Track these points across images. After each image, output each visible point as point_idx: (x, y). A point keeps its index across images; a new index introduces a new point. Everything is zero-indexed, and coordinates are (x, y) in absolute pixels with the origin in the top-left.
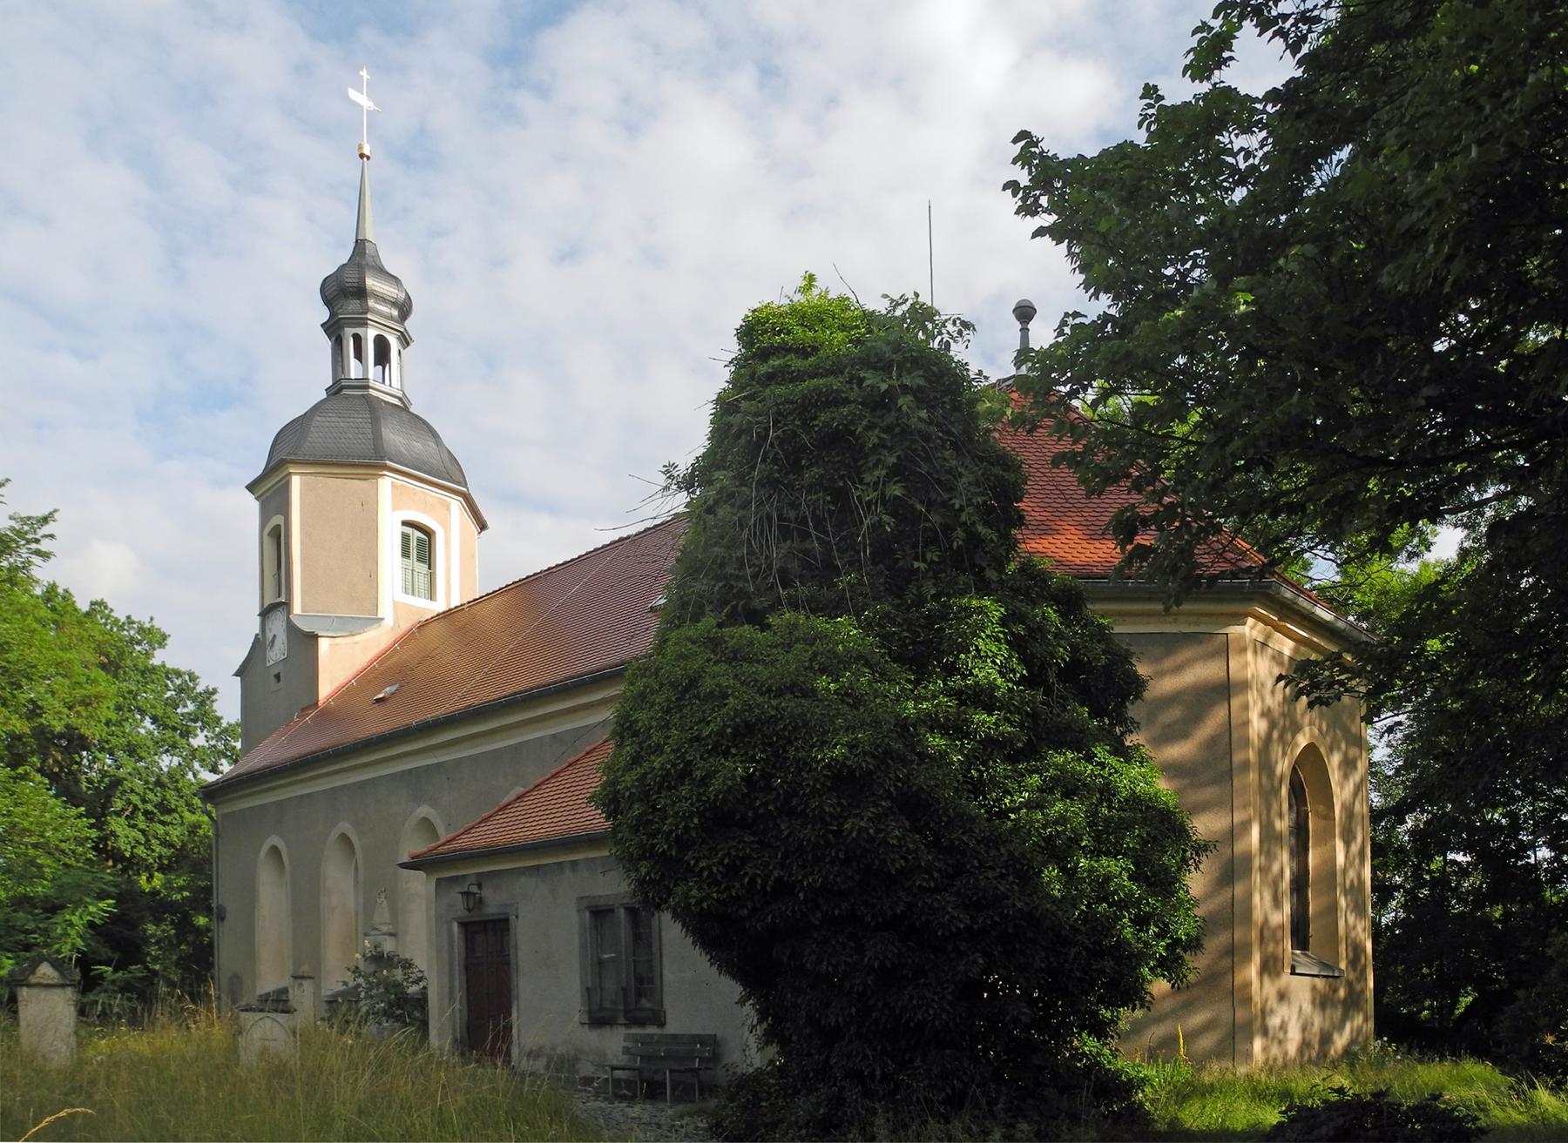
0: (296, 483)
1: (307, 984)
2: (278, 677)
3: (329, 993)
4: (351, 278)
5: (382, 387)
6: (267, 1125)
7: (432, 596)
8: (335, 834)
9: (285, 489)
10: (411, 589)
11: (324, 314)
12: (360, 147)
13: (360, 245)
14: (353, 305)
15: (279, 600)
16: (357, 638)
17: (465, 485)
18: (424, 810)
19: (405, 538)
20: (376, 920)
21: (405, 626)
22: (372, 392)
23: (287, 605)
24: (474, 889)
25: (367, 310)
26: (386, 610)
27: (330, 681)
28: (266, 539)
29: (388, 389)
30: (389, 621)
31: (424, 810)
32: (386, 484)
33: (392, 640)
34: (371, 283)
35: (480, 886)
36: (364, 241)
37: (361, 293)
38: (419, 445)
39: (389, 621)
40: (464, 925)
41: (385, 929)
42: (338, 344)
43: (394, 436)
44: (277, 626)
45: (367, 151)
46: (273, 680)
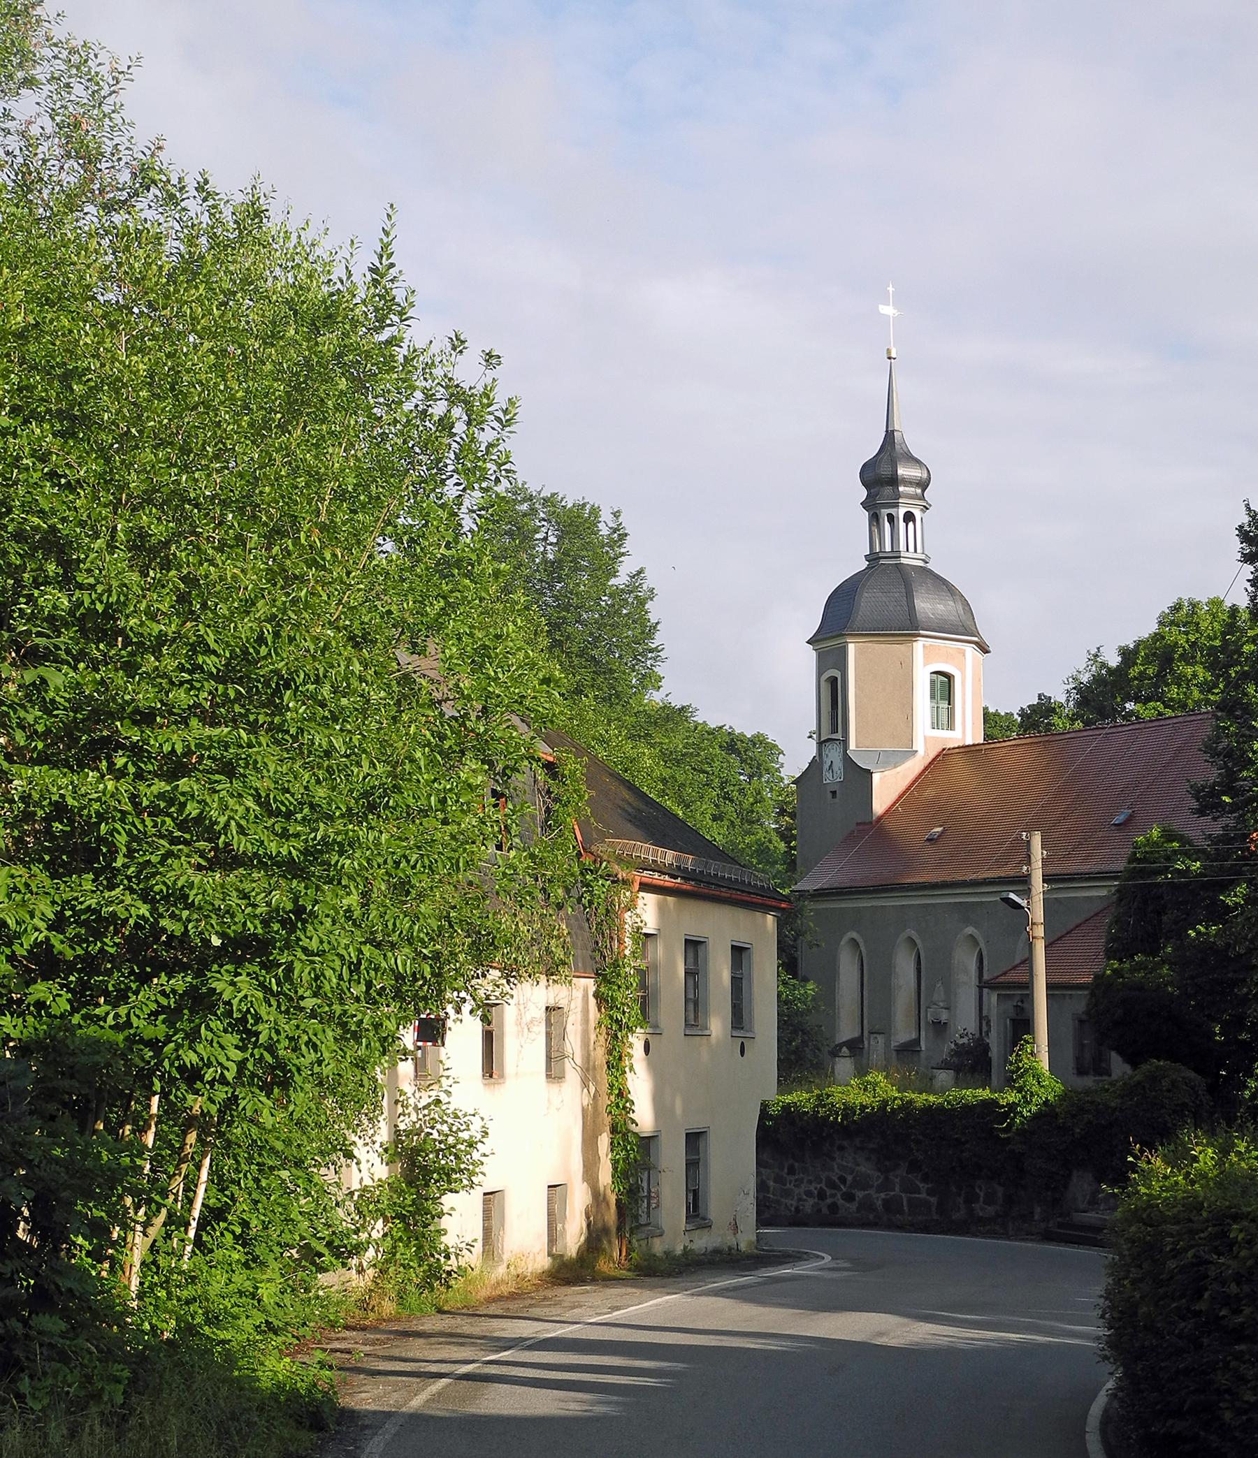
0: (851, 648)
1: (881, 1039)
2: (834, 793)
3: (897, 1044)
4: (885, 471)
5: (907, 555)
6: (179, 1203)
7: (951, 725)
8: (904, 935)
9: (843, 652)
10: (936, 725)
11: (863, 493)
12: (889, 351)
13: (890, 435)
14: (888, 490)
15: (834, 736)
16: (898, 769)
17: (977, 634)
18: (970, 930)
19: (932, 682)
20: (936, 997)
21: (932, 755)
22: (903, 561)
23: (845, 742)
24: (1019, 1004)
25: (898, 496)
26: (919, 745)
27: (881, 801)
28: (823, 684)
29: (915, 556)
30: (921, 752)
31: (970, 930)
32: (919, 646)
33: (922, 768)
34: (902, 471)
35: (1022, 1002)
36: (893, 431)
37: (894, 481)
38: (941, 607)
39: (921, 752)
40: (1013, 1020)
41: (942, 1004)
42: (875, 519)
43: (926, 605)
44: (833, 755)
45: (893, 355)
46: (830, 795)
